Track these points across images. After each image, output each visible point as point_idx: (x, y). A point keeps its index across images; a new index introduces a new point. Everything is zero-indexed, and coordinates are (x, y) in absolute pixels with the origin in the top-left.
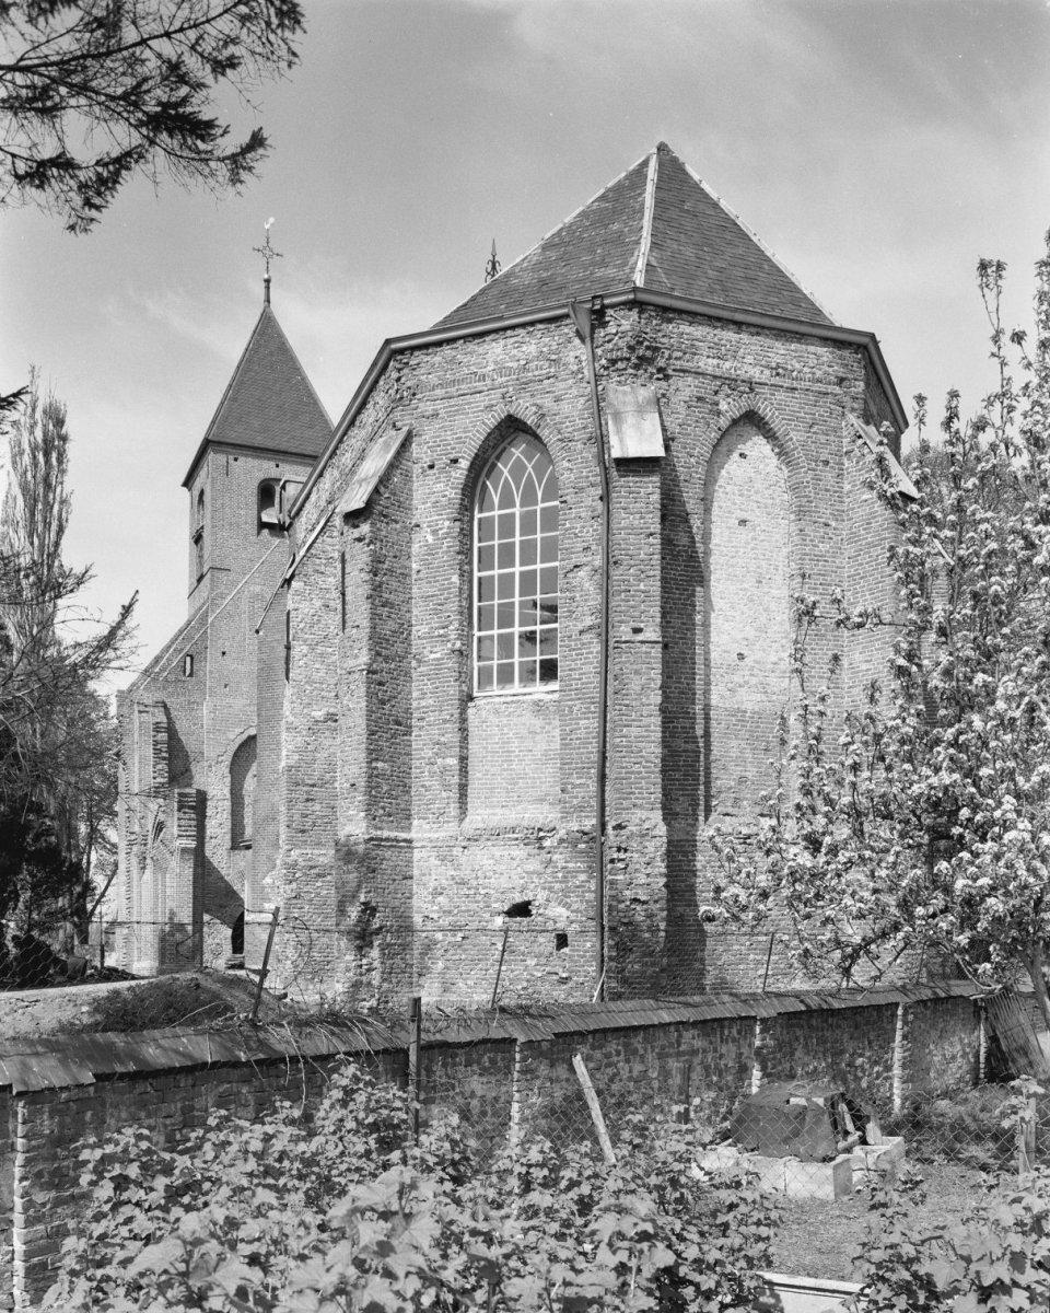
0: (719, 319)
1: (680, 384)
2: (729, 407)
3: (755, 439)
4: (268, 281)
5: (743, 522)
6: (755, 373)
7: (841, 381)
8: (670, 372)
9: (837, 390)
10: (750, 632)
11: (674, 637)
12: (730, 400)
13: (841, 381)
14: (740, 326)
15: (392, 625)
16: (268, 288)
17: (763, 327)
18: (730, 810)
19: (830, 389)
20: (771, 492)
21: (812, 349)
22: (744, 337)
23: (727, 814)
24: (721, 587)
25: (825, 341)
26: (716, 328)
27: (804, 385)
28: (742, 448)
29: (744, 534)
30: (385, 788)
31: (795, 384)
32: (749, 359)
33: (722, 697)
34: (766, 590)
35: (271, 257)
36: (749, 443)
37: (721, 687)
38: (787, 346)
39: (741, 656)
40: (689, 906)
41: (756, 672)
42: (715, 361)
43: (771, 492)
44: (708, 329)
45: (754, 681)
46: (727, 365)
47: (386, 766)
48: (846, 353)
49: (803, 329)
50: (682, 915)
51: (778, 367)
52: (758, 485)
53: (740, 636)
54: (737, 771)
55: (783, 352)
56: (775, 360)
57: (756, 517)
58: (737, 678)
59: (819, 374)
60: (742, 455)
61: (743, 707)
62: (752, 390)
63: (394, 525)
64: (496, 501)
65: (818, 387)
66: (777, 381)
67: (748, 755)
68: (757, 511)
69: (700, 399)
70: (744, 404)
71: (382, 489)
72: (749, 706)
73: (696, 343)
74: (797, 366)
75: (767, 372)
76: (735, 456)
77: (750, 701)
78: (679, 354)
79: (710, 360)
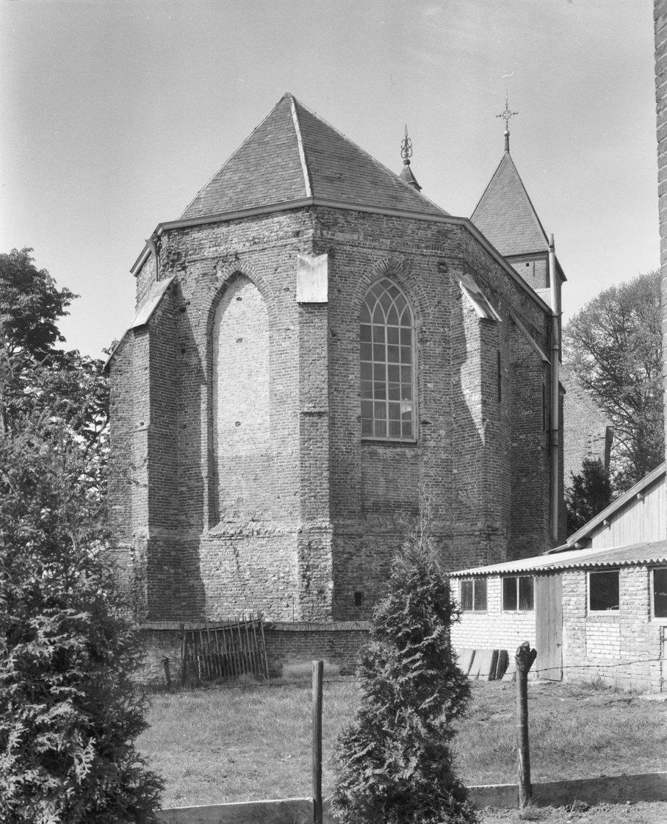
0: (214, 223)
1: (192, 270)
2: (222, 274)
3: (247, 286)
4: (507, 135)
5: (240, 340)
6: (240, 248)
7: (297, 234)
8: (187, 264)
9: (295, 240)
10: (243, 407)
11: (189, 421)
12: (224, 269)
13: (297, 234)
14: (227, 222)
15: (124, 430)
16: (507, 140)
17: (243, 218)
18: (231, 520)
19: (289, 241)
20: (257, 317)
21: (276, 219)
22: (232, 227)
23: (230, 522)
24: (224, 384)
25: (284, 211)
26: (213, 228)
27: (272, 244)
28: (237, 294)
29: (240, 348)
30: (121, 519)
31: (266, 246)
32: (235, 240)
33: (226, 450)
34: (255, 379)
35: (505, 118)
36: (243, 290)
37: (226, 446)
38: (260, 223)
39: (238, 424)
40: (197, 579)
41: (247, 431)
42: (214, 249)
43: (257, 317)
44: (209, 231)
45: (246, 437)
46: (222, 248)
47: (122, 507)
48: (300, 214)
49: (266, 210)
50: (193, 586)
51: (254, 238)
52: (249, 315)
53: (237, 411)
54: (236, 495)
55: (257, 228)
56: (251, 235)
57: (249, 335)
58: (236, 438)
59: (281, 234)
60: (239, 299)
61: (240, 455)
62: (237, 259)
63: (126, 374)
64: (372, 316)
65: (280, 243)
66: (255, 248)
67: (243, 484)
68: (248, 331)
69: (204, 275)
70: (232, 269)
71: (116, 357)
72: (243, 454)
73: (203, 242)
74: (267, 234)
75: (248, 244)
76: (234, 300)
77: (244, 450)
78: (192, 252)
79: (211, 249)
